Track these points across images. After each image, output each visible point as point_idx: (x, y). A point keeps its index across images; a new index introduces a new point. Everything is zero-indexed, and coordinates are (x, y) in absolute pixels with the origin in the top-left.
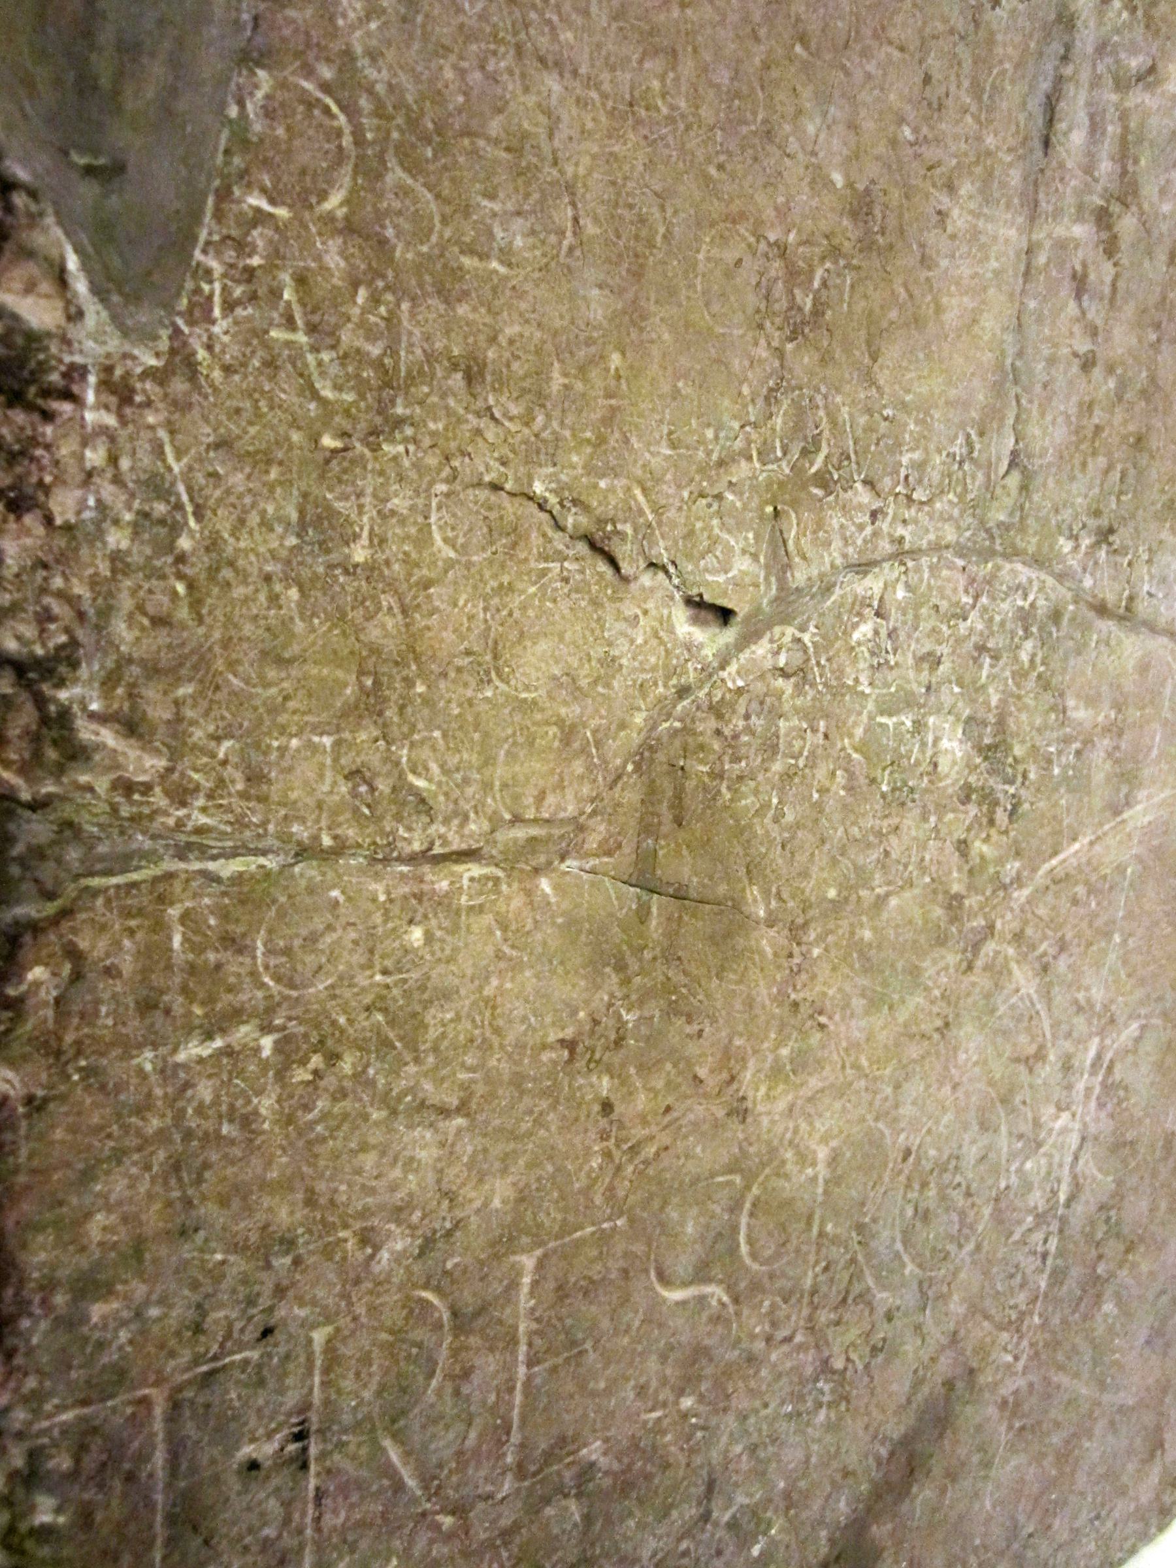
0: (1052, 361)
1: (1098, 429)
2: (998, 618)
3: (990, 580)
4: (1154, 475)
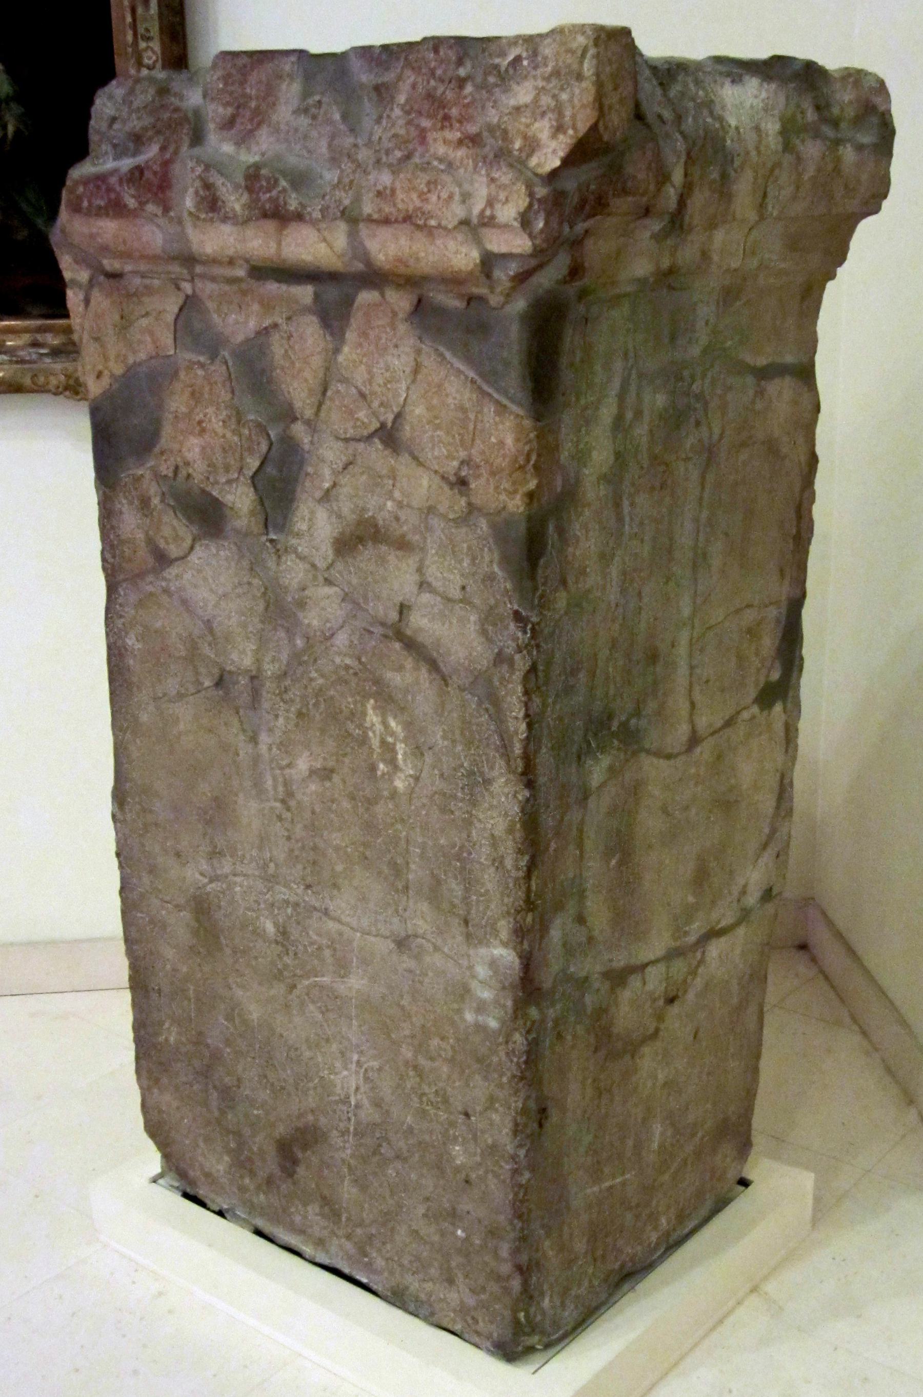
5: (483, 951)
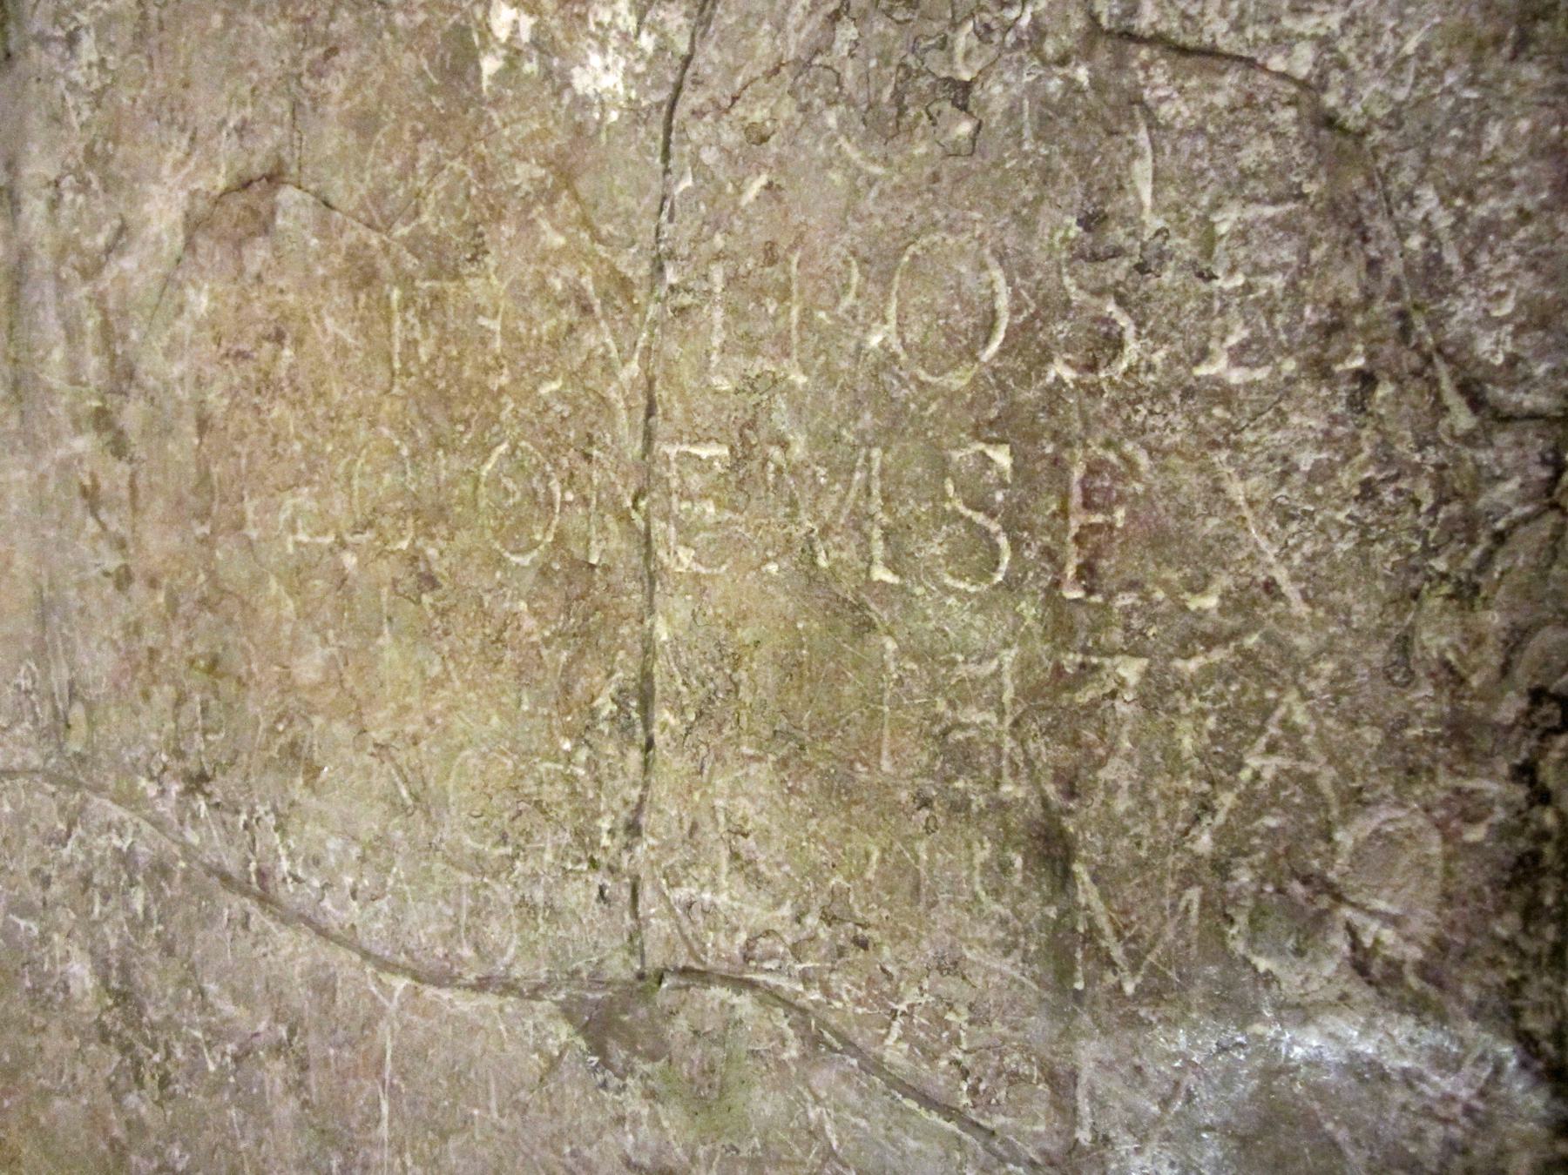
0: (82, 586)
1: (153, 653)
2: (97, 854)
3: (82, 810)
4: (253, 709)
5: (1182, 1041)
